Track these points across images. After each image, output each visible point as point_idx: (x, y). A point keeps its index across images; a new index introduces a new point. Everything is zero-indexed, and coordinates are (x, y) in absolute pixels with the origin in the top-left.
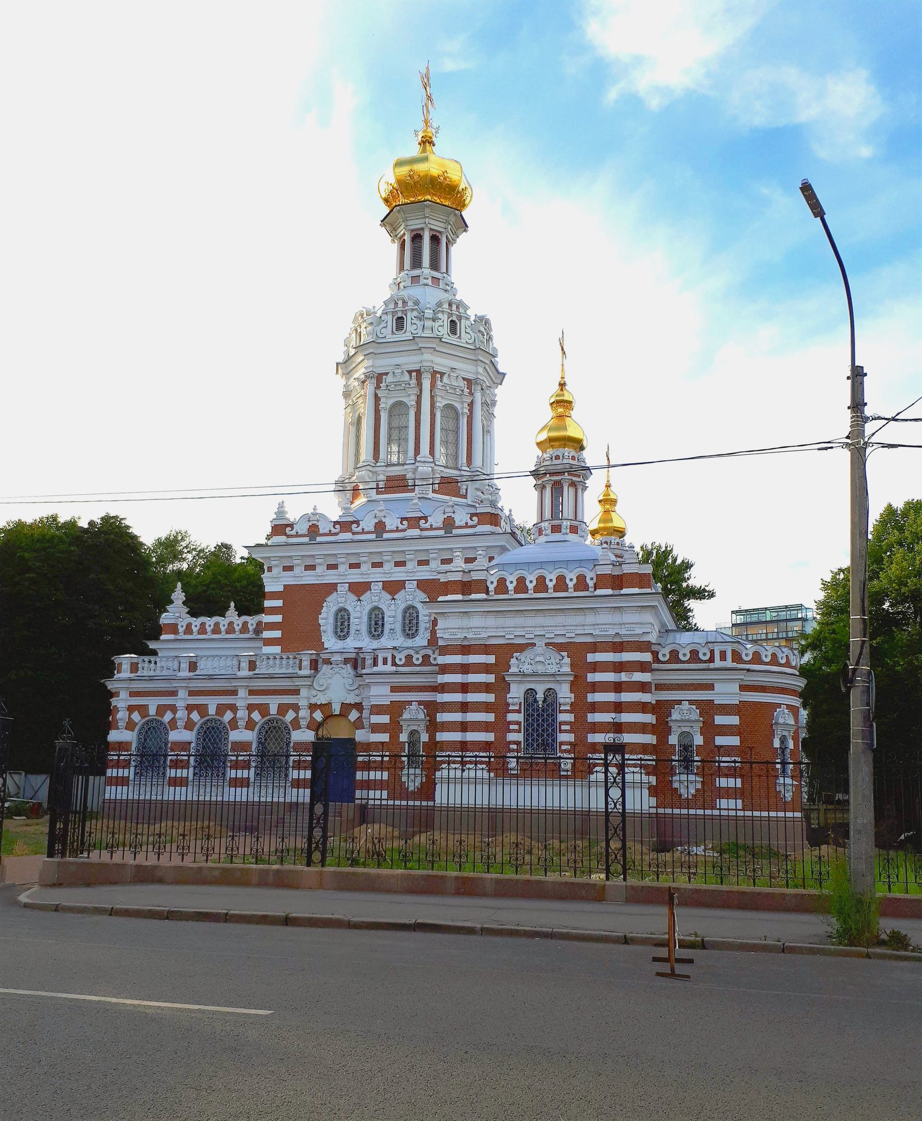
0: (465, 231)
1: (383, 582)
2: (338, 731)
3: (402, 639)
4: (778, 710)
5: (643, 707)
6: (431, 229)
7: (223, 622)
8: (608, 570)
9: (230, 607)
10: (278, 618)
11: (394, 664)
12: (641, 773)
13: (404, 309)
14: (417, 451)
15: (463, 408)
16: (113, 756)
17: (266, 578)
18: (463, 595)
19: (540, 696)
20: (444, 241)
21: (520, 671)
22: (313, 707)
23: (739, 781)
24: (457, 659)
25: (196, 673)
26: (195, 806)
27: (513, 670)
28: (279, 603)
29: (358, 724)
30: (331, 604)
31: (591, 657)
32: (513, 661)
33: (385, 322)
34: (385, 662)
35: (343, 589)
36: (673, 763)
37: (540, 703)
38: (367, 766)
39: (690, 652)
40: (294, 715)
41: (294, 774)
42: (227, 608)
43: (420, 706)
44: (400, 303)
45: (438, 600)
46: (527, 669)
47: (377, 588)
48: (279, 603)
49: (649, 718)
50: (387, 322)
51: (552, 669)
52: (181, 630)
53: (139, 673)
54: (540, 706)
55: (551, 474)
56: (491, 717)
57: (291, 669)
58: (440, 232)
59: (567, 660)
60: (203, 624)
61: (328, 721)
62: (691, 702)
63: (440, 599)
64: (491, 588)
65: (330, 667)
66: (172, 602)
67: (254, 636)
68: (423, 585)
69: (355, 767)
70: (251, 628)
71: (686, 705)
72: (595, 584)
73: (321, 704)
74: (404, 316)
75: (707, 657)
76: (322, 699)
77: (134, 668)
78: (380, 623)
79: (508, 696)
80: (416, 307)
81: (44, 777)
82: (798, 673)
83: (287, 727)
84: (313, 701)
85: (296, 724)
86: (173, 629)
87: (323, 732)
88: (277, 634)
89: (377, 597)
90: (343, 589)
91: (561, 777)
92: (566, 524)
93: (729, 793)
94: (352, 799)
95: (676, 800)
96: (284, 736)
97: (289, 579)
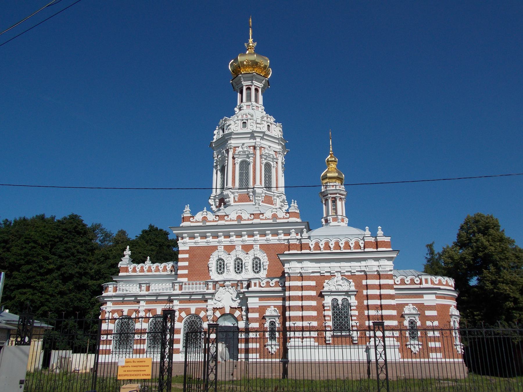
4: (451, 308)
6: (255, 86)
9: (147, 259)
15: (274, 164)
16: (104, 337)
17: (180, 243)
19: (340, 302)
21: (329, 289)
22: (215, 309)
23: (258, 345)
25: (116, 293)
26: (110, 365)
27: (326, 289)
28: (187, 256)
30: (214, 257)
34: (255, 285)
37: (340, 306)
39: (410, 279)
43: (275, 308)
45: (285, 253)
48: (187, 256)
51: (346, 288)
52: (130, 270)
53: (183, 291)
54: (340, 307)
55: (339, 194)
58: (259, 87)
59: (353, 284)
61: (229, 316)
62: (413, 304)
64: (312, 247)
65: (224, 288)
66: (124, 256)
68: (264, 247)
70: (168, 269)
71: (411, 306)
72: (364, 246)
73: (219, 308)
75: (418, 282)
76: (219, 305)
77: (115, 290)
78: (240, 266)
80: (252, 118)
81: (356, 302)
82: (454, 289)
84: (215, 306)
86: (126, 269)
89: (239, 252)
91: (327, 344)
92: (340, 217)
93: (435, 350)
95: (412, 354)
96: (198, 325)
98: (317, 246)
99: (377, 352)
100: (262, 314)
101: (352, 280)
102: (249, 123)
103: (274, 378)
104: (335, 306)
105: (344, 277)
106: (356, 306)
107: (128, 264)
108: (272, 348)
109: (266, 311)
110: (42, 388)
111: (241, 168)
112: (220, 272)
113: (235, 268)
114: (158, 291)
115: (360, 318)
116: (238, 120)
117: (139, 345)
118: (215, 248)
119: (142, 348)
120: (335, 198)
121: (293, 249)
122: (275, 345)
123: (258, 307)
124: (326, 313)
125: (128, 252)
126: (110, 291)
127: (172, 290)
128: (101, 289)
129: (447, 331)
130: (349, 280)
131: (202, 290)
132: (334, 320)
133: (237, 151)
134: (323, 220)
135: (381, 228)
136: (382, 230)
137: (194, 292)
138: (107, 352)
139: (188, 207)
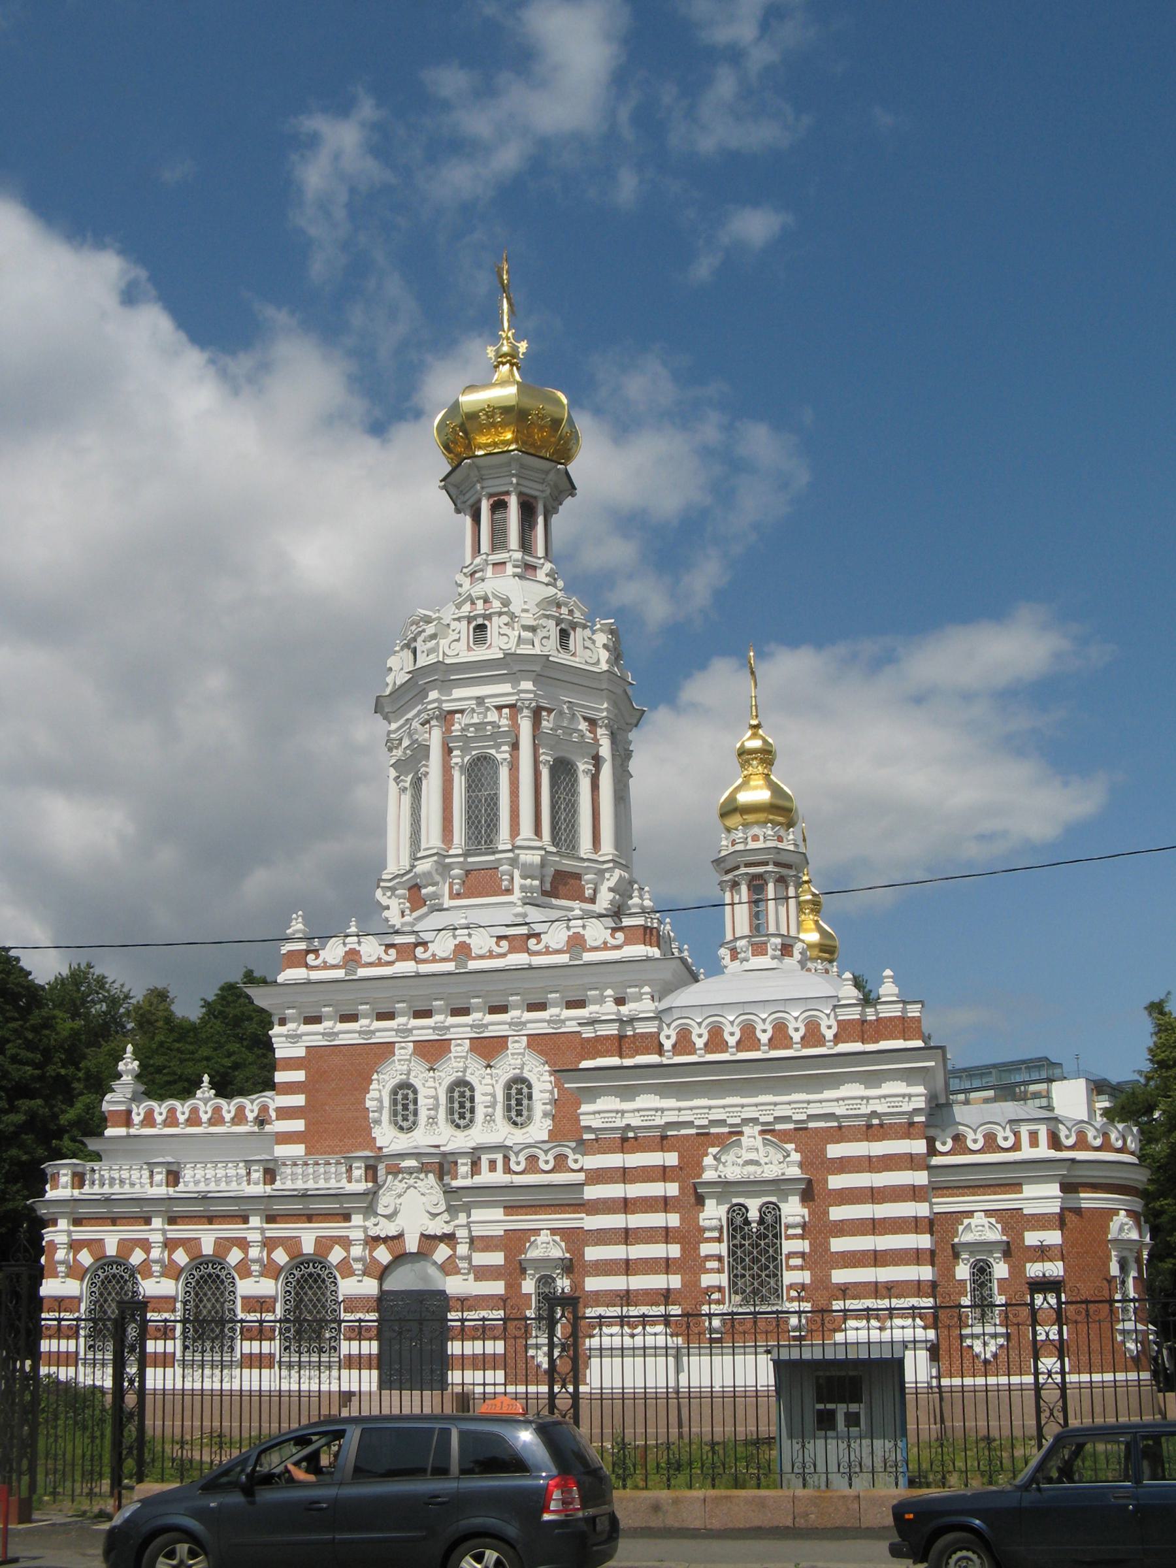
0: (573, 495)
1: (470, 1038)
2: (403, 1280)
3: (508, 1128)
5: (914, 1225)
7: (182, 1109)
8: (854, 1014)
10: (299, 1100)
11: (508, 1170)
12: (666, 1334)
13: (487, 612)
14: (515, 830)
18: (621, 1057)
19: (754, 1215)
20: (540, 509)
22: (374, 1241)
24: (614, 1160)
25: (274, 1187)
26: (255, 1399)
27: (709, 1175)
28: (299, 1076)
29: (449, 1268)
31: (835, 1151)
32: (708, 1160)
33: (457, 631)
35: (404, 1052)
36: (528, 1322)
38: (464, 1334)
40: (242, 1256)
41: (348, 1347)
42: (198, 1084)
44: (480, 603)
46: (733, 1173)
47: (460, 1049)
48: (299, 1076)
49: (924, 1241)
50: (459, 633)
51: (771, 1171)
52: (136, 1119)
54: (754, 1230)
56: (674, 1251)
57: (300, 1182)
58: (535, 498)
59: (796, 1157)
60: (172, 1111)
63: (585, 1064)
66: (119, 1076)
67: (256, 1129)
68: (537, 1042)
69: (444, 1334)
70: (251, 1116)
74: (486, 622)
76: (388, 1229)
77: (79, 1179)
79: (702, 1216)
80: (505, 609)
83: (331, 1273)
85: (346, 1268)
87: (391, 1284)
88: (298, 1125)
90: (404, 1052)
94: (443, 1384)
96: (326, 1287)
97: (314, 1035)
98: (684, 1043)
99: (1040, 1365)
100: (515, 1256)
101: (793, 1146)
102: (495, 626)
103: (741, 1437)
104: (737, 1224)
105: (768, 1137)
106: (804, 1226)
107: (133, 1099)
108: (985, 1344)
109: (528, 1244)
110: (64, 1455)
111: (473, 781)
112: (405, 1124)
113: (452, 1113)
114: (202, 1187)
115: (815, 1263)
116: (458, 619)
117: (63, 1349)
118: (387, 1049)
119: (266, 1350)
120: (760, 876)
121: (638, 1052)
122: (995, 1336)
123: (502, 1233)
124: (804, 1246)
125: (129, 1065)
126: (60, 1190)
127: (345, 1180)
128: (37, 1182)
129: (1100, 1306)
130: (785, 1145)
131: (333, 1183)
132: (731, 1268)
133: (457, 727)
134: (724, 952)
135: (892, 974)
136: (896, 980)
137: (209, 1192)
138: (165, 1360)
139: (300, 920)
